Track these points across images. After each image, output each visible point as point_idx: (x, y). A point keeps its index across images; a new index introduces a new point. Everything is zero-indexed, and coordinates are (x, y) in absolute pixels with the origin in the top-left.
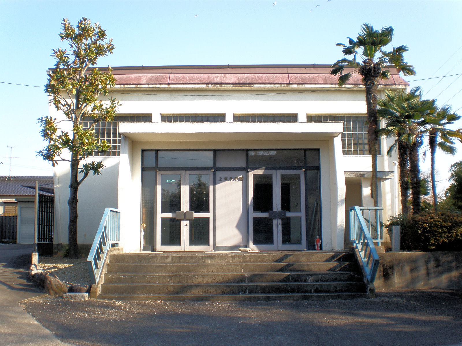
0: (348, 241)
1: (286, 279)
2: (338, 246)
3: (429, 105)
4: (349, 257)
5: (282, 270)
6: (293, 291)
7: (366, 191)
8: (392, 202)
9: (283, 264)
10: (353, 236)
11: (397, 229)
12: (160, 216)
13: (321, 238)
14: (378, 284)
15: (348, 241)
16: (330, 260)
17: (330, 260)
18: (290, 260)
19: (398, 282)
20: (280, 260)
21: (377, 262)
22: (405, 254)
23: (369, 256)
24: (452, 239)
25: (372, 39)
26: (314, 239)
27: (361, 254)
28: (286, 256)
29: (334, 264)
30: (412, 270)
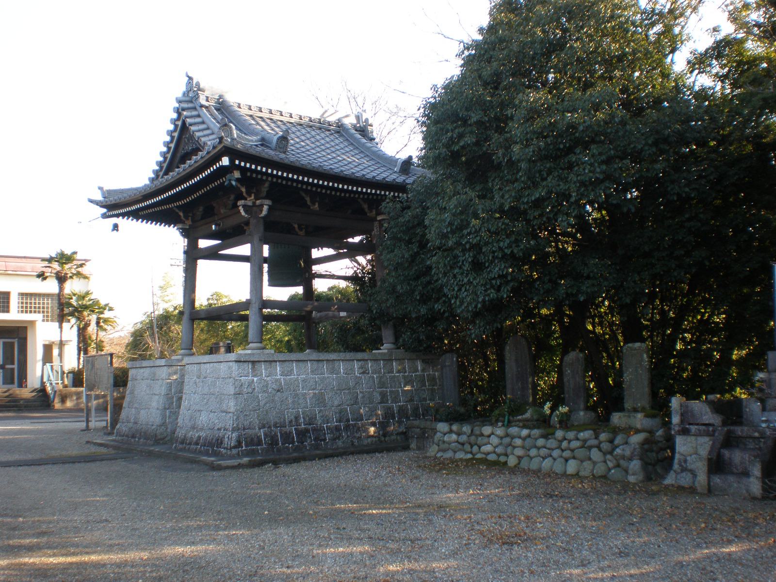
0: (43, 383)
1: (9, 402)
2: (37, 385)
3: (96, 303)
4: (43, 390)
5: (7, 397)
6: (13, 407)
7: (56, 352)
8: (71, 360)
9: (7, 394)
10: (45, 380)
11: (71, 375)
12: (15, 366)
13: (26, 381)
14: (57, 405)
15: (43, 383)
16: (32, 392)
17: (32, 392)
18: (11, 392)
19: (69, 404)
20: (5, 392)
21: (55, 392)
22: (74, 389)
23: (53, 389)
24: (685, 579)
25: (64, 259)
26: (22, 380)
27: (49, 389)
28: (8, 390)
29: (34, 394)
30: (77, 399)
